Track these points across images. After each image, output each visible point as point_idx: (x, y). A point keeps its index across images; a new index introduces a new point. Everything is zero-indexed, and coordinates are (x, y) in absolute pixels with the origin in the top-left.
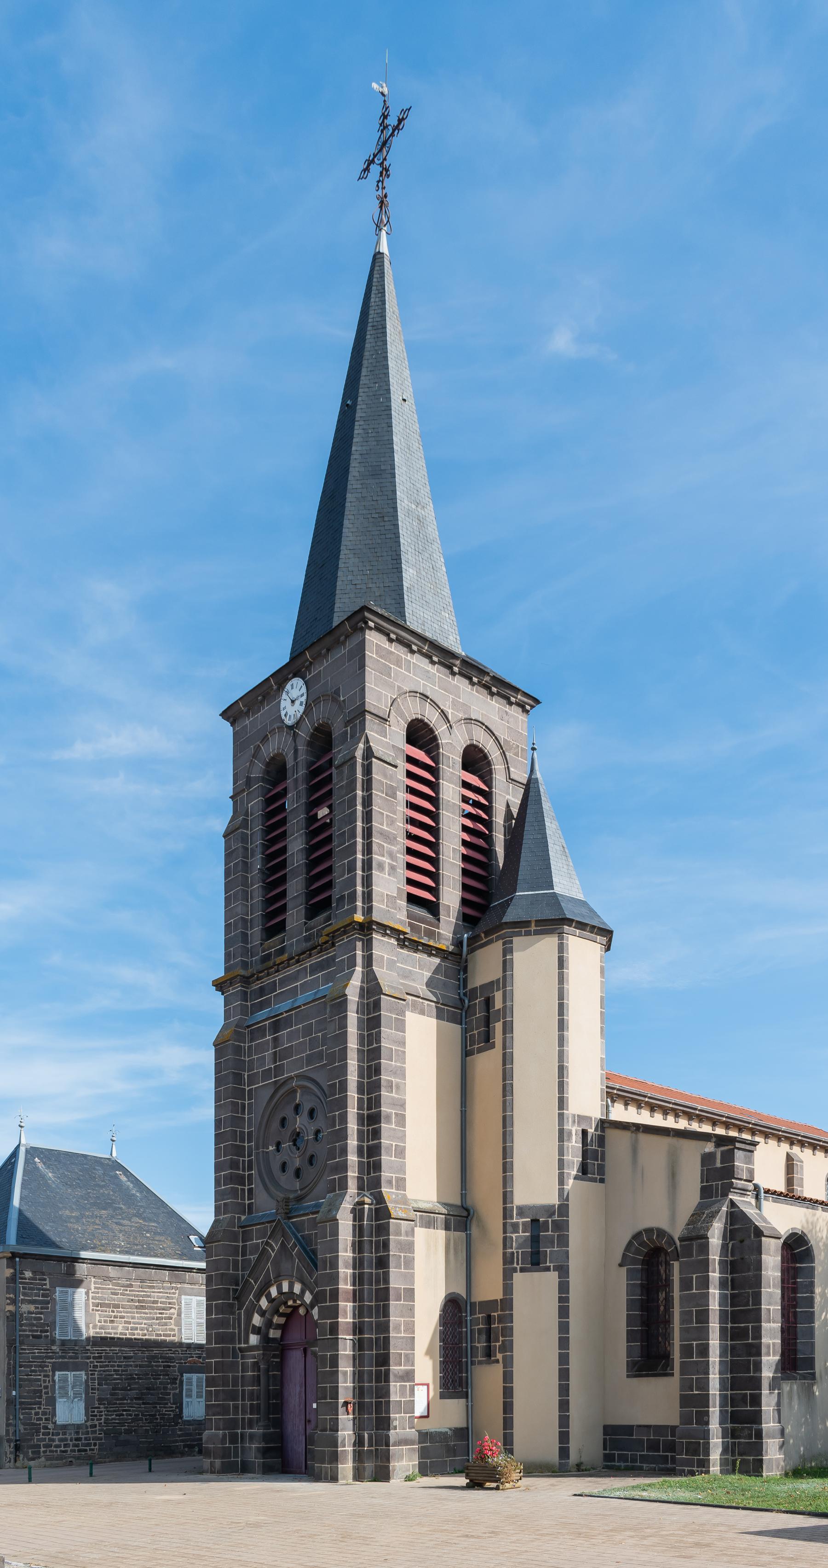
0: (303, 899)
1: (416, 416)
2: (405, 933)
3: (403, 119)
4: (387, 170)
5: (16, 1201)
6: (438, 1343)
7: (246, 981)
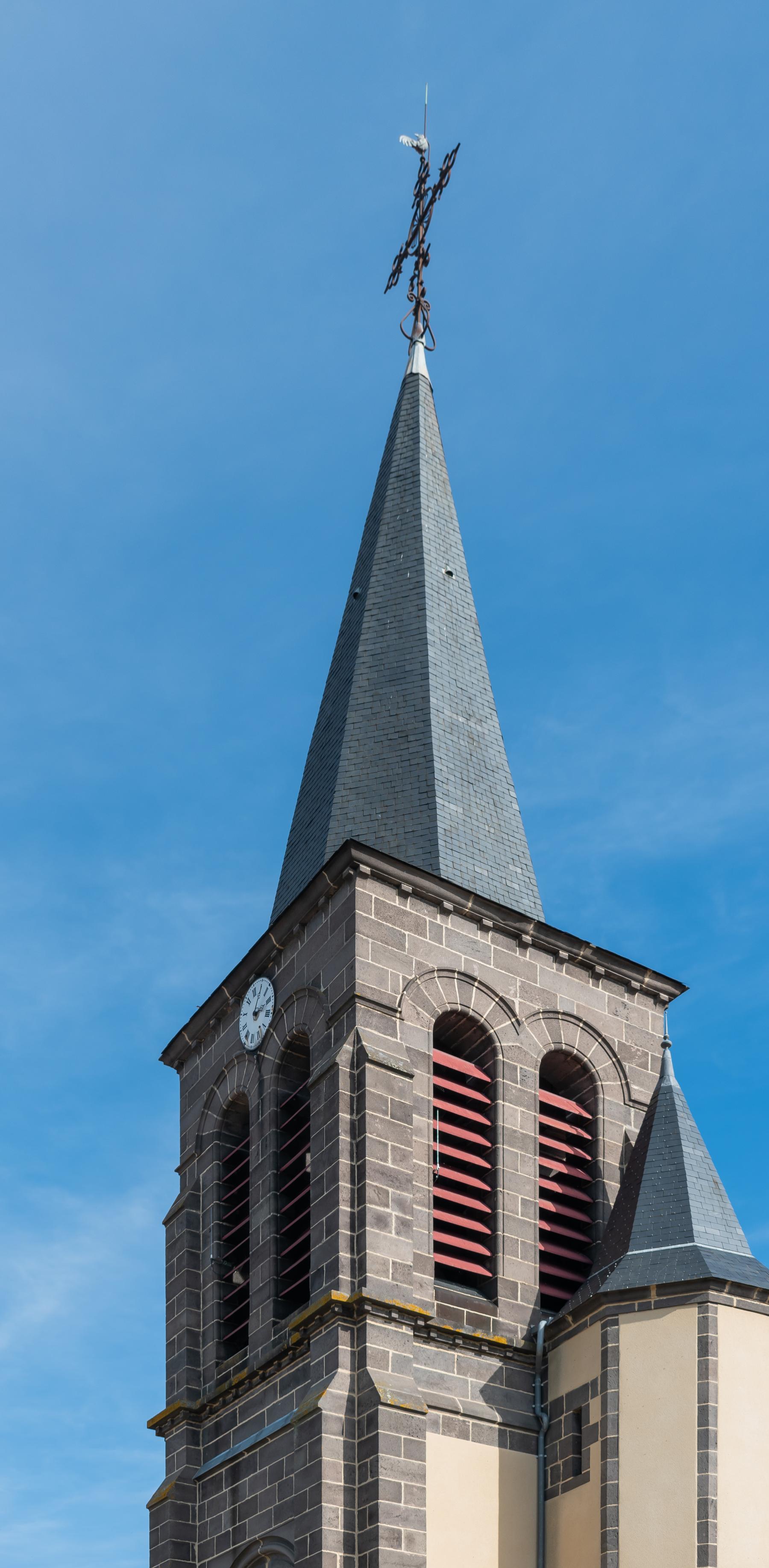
0: (270, 1289)
1: (470, 596)
2: (426, 1318)
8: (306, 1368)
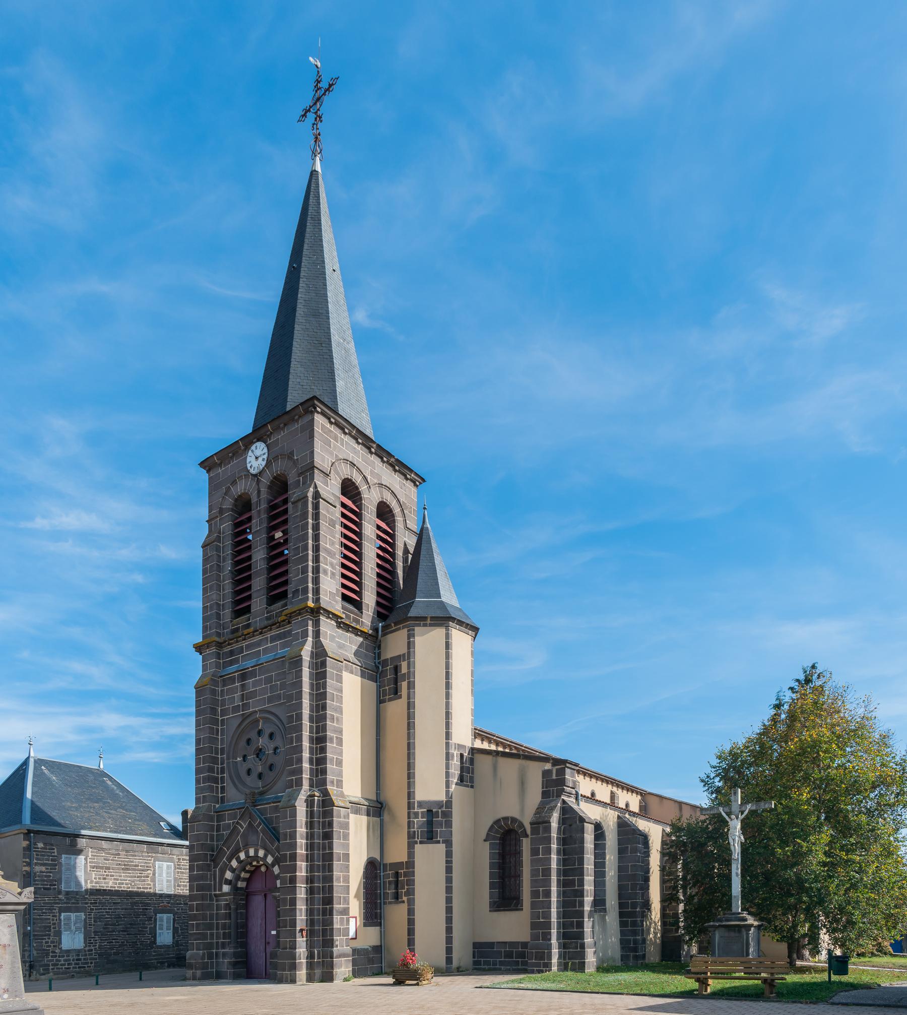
2: (342, 618)
3: (303, 116)
4: (320, 117)
5: (29, 794)
6: (362, 890)
7: (220, 645)
8: (289, 632)
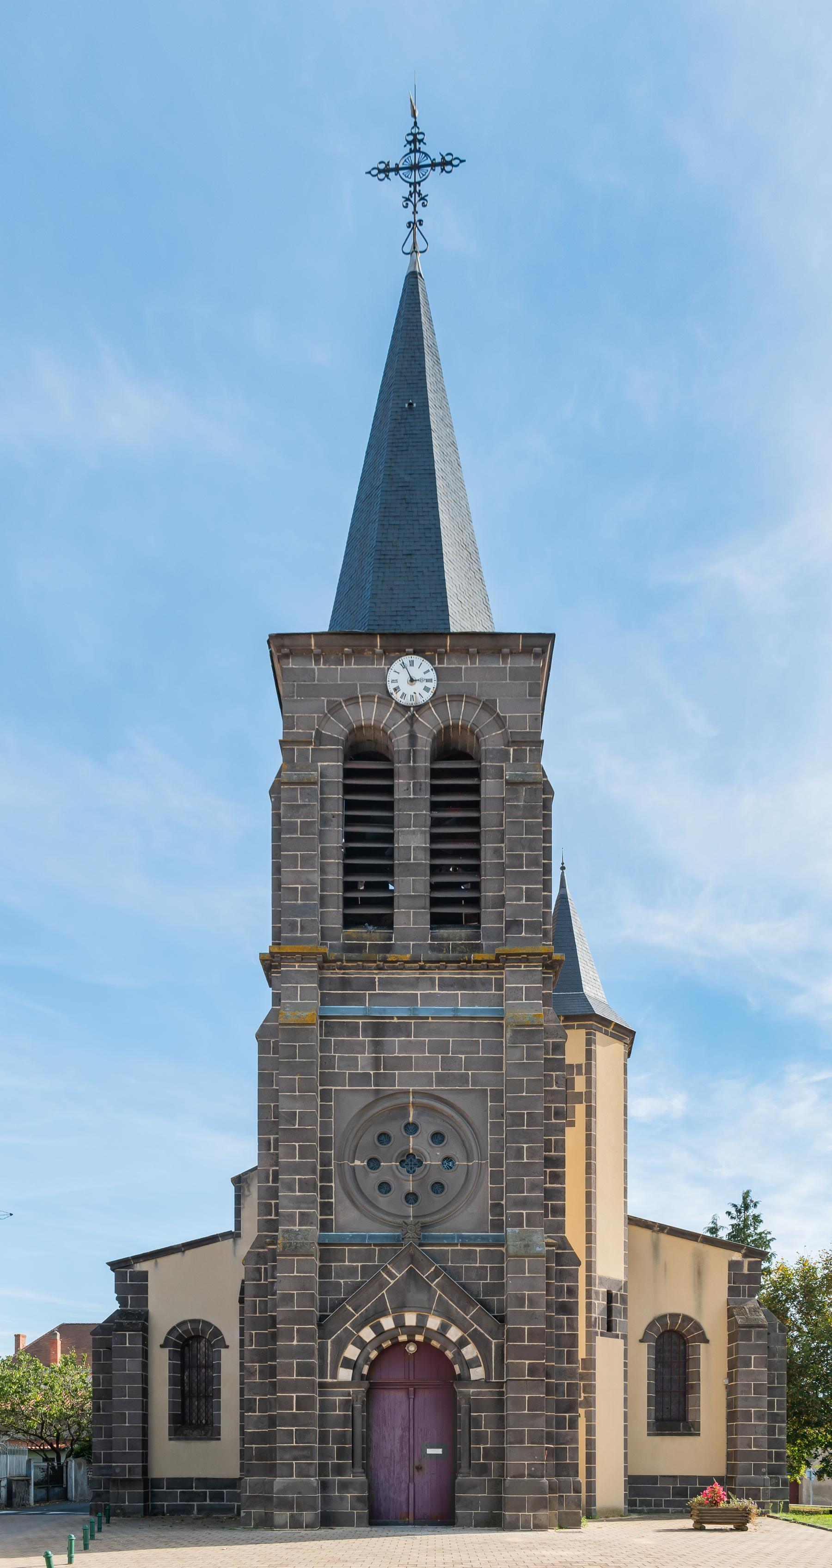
7: (325, 962)
